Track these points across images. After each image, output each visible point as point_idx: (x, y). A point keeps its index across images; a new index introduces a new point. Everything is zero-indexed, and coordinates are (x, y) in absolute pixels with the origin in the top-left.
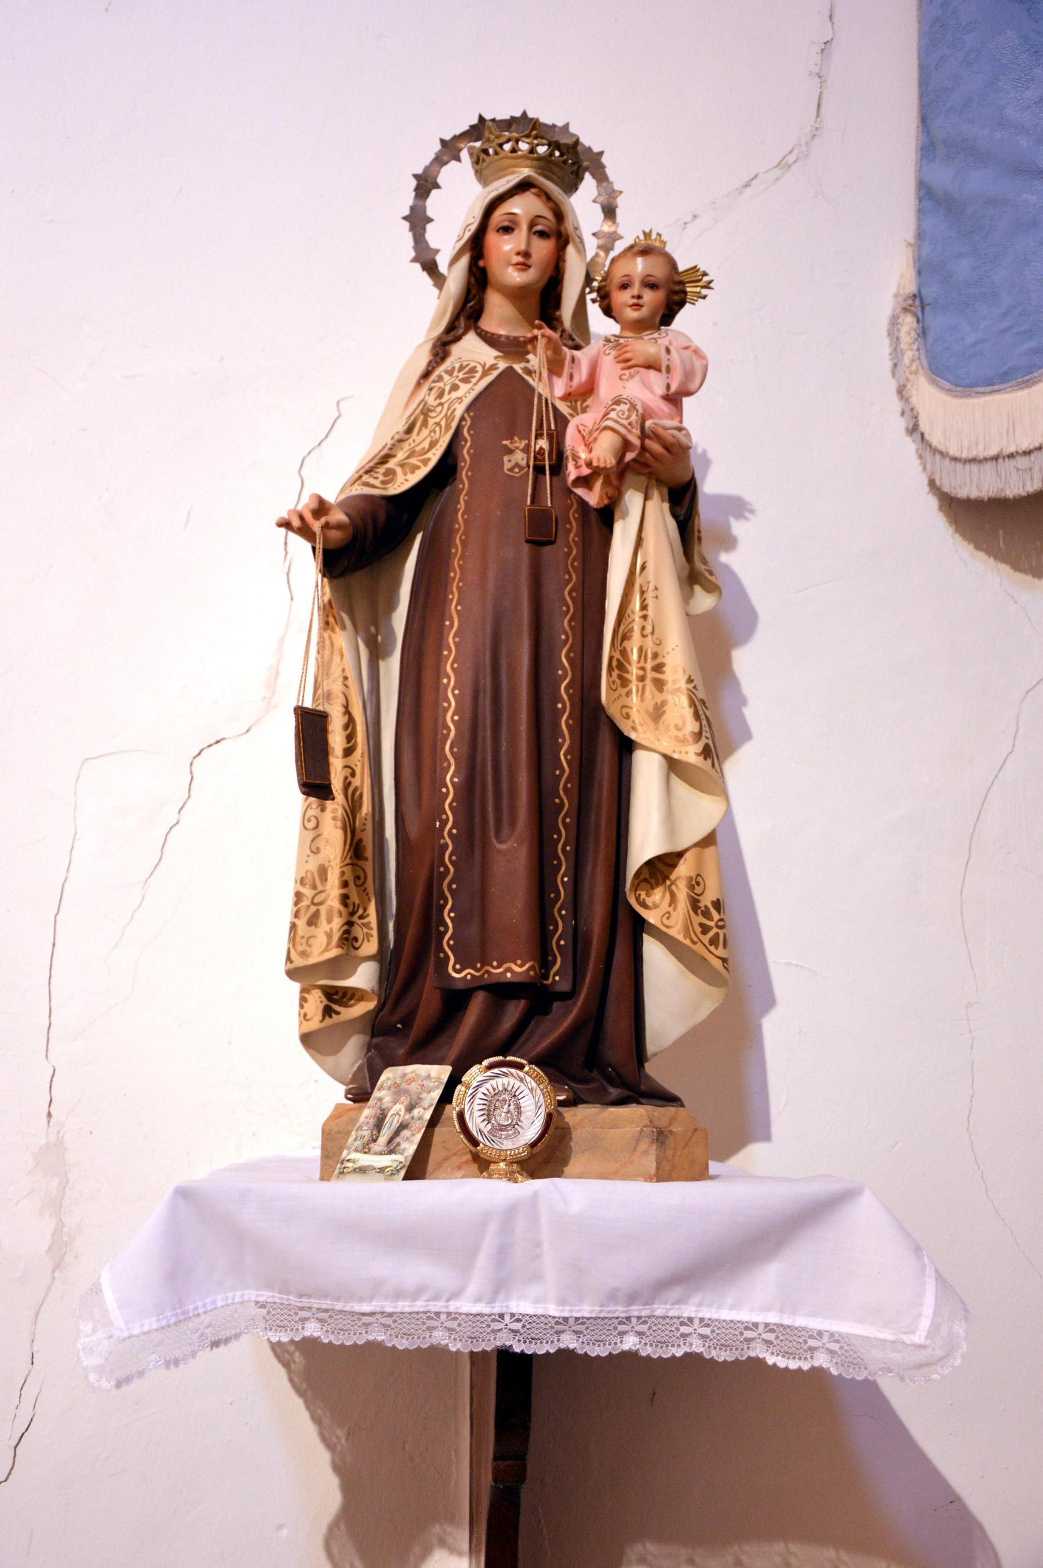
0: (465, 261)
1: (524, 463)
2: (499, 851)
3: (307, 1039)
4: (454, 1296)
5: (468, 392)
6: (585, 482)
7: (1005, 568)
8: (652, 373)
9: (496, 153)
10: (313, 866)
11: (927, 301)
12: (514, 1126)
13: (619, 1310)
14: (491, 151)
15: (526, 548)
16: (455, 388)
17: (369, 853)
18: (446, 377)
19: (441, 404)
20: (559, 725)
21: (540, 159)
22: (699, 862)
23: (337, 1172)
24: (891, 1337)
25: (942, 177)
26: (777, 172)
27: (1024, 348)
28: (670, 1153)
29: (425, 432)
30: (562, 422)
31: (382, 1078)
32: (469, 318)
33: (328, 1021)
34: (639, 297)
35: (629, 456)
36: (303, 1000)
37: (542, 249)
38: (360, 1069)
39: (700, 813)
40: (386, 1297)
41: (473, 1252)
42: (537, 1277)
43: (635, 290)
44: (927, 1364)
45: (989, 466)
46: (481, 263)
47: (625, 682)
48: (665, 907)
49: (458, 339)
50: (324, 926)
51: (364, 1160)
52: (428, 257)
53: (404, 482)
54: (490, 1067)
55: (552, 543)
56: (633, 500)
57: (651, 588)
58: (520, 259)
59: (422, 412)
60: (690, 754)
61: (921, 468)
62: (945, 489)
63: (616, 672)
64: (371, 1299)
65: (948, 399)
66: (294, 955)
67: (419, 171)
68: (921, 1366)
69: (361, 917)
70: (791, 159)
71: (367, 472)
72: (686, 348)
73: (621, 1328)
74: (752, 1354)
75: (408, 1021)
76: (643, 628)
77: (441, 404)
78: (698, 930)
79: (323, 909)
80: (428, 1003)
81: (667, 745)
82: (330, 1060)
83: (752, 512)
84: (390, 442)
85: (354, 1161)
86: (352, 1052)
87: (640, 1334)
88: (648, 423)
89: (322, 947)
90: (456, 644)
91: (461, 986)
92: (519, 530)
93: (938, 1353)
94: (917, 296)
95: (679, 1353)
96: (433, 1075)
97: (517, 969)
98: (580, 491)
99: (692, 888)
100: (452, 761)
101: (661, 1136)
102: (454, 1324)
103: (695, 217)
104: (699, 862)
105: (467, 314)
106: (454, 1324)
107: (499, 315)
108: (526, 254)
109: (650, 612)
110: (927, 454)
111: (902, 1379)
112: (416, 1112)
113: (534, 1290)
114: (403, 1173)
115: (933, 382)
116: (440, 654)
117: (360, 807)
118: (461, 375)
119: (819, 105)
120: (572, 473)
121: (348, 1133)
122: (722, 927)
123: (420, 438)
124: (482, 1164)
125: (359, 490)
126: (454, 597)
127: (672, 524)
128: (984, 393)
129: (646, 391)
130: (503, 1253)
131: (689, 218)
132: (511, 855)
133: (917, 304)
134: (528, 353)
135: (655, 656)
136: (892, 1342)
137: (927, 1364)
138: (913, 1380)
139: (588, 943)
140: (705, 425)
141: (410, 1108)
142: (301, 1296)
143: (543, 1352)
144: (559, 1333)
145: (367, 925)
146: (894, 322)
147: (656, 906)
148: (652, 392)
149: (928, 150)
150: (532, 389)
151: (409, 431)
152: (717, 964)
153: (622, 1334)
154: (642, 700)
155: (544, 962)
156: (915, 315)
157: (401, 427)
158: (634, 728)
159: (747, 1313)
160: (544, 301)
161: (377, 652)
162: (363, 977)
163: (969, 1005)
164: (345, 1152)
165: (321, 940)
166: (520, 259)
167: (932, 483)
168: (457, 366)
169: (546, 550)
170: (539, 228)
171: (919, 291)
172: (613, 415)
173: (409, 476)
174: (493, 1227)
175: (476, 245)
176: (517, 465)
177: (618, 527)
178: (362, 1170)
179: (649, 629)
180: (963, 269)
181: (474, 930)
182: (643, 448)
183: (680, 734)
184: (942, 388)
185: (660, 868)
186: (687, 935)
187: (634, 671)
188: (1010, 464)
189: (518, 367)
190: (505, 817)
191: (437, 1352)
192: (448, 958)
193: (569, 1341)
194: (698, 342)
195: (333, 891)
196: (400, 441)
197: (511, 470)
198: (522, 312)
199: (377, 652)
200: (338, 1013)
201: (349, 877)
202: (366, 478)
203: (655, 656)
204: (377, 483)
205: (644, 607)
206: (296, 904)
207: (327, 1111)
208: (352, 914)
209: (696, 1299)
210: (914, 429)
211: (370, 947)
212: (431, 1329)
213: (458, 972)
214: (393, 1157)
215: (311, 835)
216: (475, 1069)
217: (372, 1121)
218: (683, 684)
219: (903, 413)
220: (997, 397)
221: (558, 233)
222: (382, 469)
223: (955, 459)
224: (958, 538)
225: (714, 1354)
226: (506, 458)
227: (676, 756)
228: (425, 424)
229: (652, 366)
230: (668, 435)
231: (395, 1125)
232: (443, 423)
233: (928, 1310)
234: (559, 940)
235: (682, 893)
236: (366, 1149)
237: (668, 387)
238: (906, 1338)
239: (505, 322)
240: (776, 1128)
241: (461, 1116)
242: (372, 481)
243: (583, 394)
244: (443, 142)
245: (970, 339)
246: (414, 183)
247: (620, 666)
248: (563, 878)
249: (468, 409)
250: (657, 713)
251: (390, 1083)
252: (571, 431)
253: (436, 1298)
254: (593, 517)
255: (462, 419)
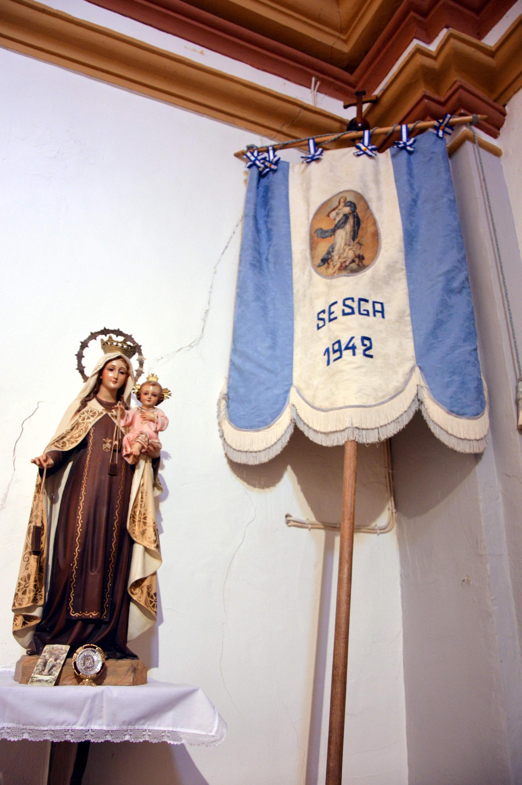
0: (96, 377)
1: (109, 447)
2: (91, 576)
3: (15, 633)
4: (74, 724)
5: (93, 421)
6: (128, 456)
7: (245, 484)
8: (152, 423)
9: (111, 345)
10: (26, 574)
11: (230, 397)
12: (93, 667)
13: (125, 728)
14: (109, 343)
15: (108, 476)
16: (89, 418)
17: (44, 571)
18: (86, 414)
19: (83, 423)
20: (113, 535)
21: (125, 349)
22: (151, 581)
23: (30, 681)
24: (205, 734)
25: (238, 361)
26: (189, 348)
27: (257, 420)
28: (137, 675)
29: (77, 431)
30: (123, 435)
31: (45, 649)
32: (94, 393)
33: (24, 627)
34: (150, 398)
35: (143, 451)
36: (15, 619)
37: (122, 377)
38: (31, 643)
39: (153, 564)
40: (53, 725)
41: (82, 709)
42: (100, 718)
43: (149, 396)
44: (215, 741)
45: (244, 454)
46: (101, 377)
47: (134, 522)
48: (139, 594)
49: (90, 400)
50: (28, 595)
51: (40, 677)
52: (82, 369)
53: (69, 447)
54: (85, 648)
55: (116, 475)
56: (142, 463)
57: (145, 492)
58: (114, 380)
59: (76, 424)
60: (152, 547)
61: (223, 449)
62: (231, 458)
63: (132, 519)
64: (48, 725)
65: (234, 430)
66: (16, 604)
67: (83, 341)
68: (213, 742)
69: (40, 592)
70: (193, 345)
71: (56, 442)
72: (163, 416)
73: (125, 733)
74: (163, 740)
75: (52, 628)
76: (141, 505)
77: (83, 423)
78: (149, 602)
79: (28, 589)
80: (61, 623)
81: (146, 544)
82: (21, 639)
83: (170, 457)
84: (65, 433)
85: (36, 678)
86: (28, 638)
87: (130, 735)
88: (150, 441)
89: (26, 602)
90: (83, 505)
91: (73, 618)
92: (106, 470)
93: (218, 738)
94: (227, 394)
95: (142, 740)
96: (63, 648)
97: (94, 615)
98: (126, 459)
99: (148, 589)
100: (78, 544)
101: (135, 670)
102: (73, 733)
103: (162, 358)
104: (151, 581)
105: (94, 392)
106: (73, 733)
107: (104, 394)
108: (117, 379)
109: (144, 500)
110: (226, 445)
111: (207, 746)
112: (58, 661)
113: (99, 722)
114: (54, 683)
115: (230, 423)
116: (77, 508)
117: (43, 554)
118: (91, 414)
119: (203, 329)
120: (124, 453)
121: (33, 668)
122: (156, 602)
123: (75, 433)
124: (79, 679)
125: (54, 448)
126: (83, 489)
127: (152, 470)
128: (245, 431)
129: (148, 429)
130: (91, 710)
131: (160, 358)
132: (94, 576)
133: (227, 397)
134: (112, 409)
135: (144, 514)
136: (205, 735)
137: (215, 741)
138: (210, 746)
139: (115, 606)
140: (166, 442)
141: (56, 660)
142: (24, 725)
143: (100, 741)
144: (106, 735)
145: (41, 595)
146: (219, 401)
147: (136, 594)
148: (151, 429)
149: (234, 350)
150: (115, 424)
151: (72, 429)
152: (154, 613)
153: (125, 735)
154: (139, 528)
155: (102, 612)
156: (226, 400)
157: (69, 427)
158: (136, 537)
159: (162, 727)
160: (119, 393)
161: (53, 501)
162: (38, 612)
163: (223, 624)
164: (33, 674)
165: (27, 600)
166: (114, 380)
167: (226, 455)
168: (90, 410)
169: (114, 477)
170: (121, 371)
171: (228, 393)
172: (140, 438)
173: (70, 445)
174: (89, 702)
175: (101, 372)
176: (107, 448)
177: (137, 472)
178: (40, 681)
179: (143, 505)
180: (242, 391)
181: (80, 600)
182: (148, 448)
183: (150, 540)
184: (232, 426)
185: (139, 583)
186: (146, 604)
187: (137, 518)
188: (251, 454)
189: (109, 414)
190: (94, 563)
191: (67, 743)
192: (70, 609)
193: (109, 738)
194: (167, 415)
195: (32, 582)
196: (69, 432)
197: (105, 449)
198: (112, 395)
199: (53, 501)
200: (27, 624)
201: (37, 579)
202: (56, 443)
203: (144, 514)
204: (60, 446)
205: (142, 498)
206: (19, 587)
207: (18, 658)
208: (37, 591)
209: (148, 723)
210: (222, 436)
211: (41, 602)
212: (65, 735)
213: (73, 614)
214: (51, 676)
215: (25, 563)
216: (80, 648)
217: (42, 664)
218: (152, 524)
219: (219, 431)
220: (248, 433)
221: (126, 372)
222: (61, 441)
223: (234, 449)
224: (232, 472)
225: (152, 740)
226: (104, 445)
227: (148, 547)
228: (77, 428)
229: (152, 421)
230: (155, 445)
231: (51, 665)
232: (84, 429)
233: (216, 725)
234: (106, 605)
235: (145, 590)
236: (40, 673)
237: (156, 428)
238: (209, 734)
239: (105, 397)
240: (160, 663)
241: (75, 663)
242: (58, 445)
243: (129, 426)
244: (92, 333)
245: (242, 413)
246: (80, 344)
247: (133, 516)
248: (109, 585)
249: (93, 427)
250: (143, 533)
251: (48, 650)
252: (125, 439)
253: (68, 725)
254: (129, 467)
255: (91, 429)
